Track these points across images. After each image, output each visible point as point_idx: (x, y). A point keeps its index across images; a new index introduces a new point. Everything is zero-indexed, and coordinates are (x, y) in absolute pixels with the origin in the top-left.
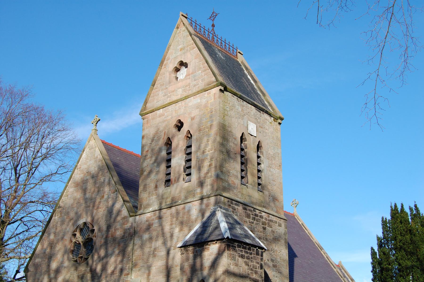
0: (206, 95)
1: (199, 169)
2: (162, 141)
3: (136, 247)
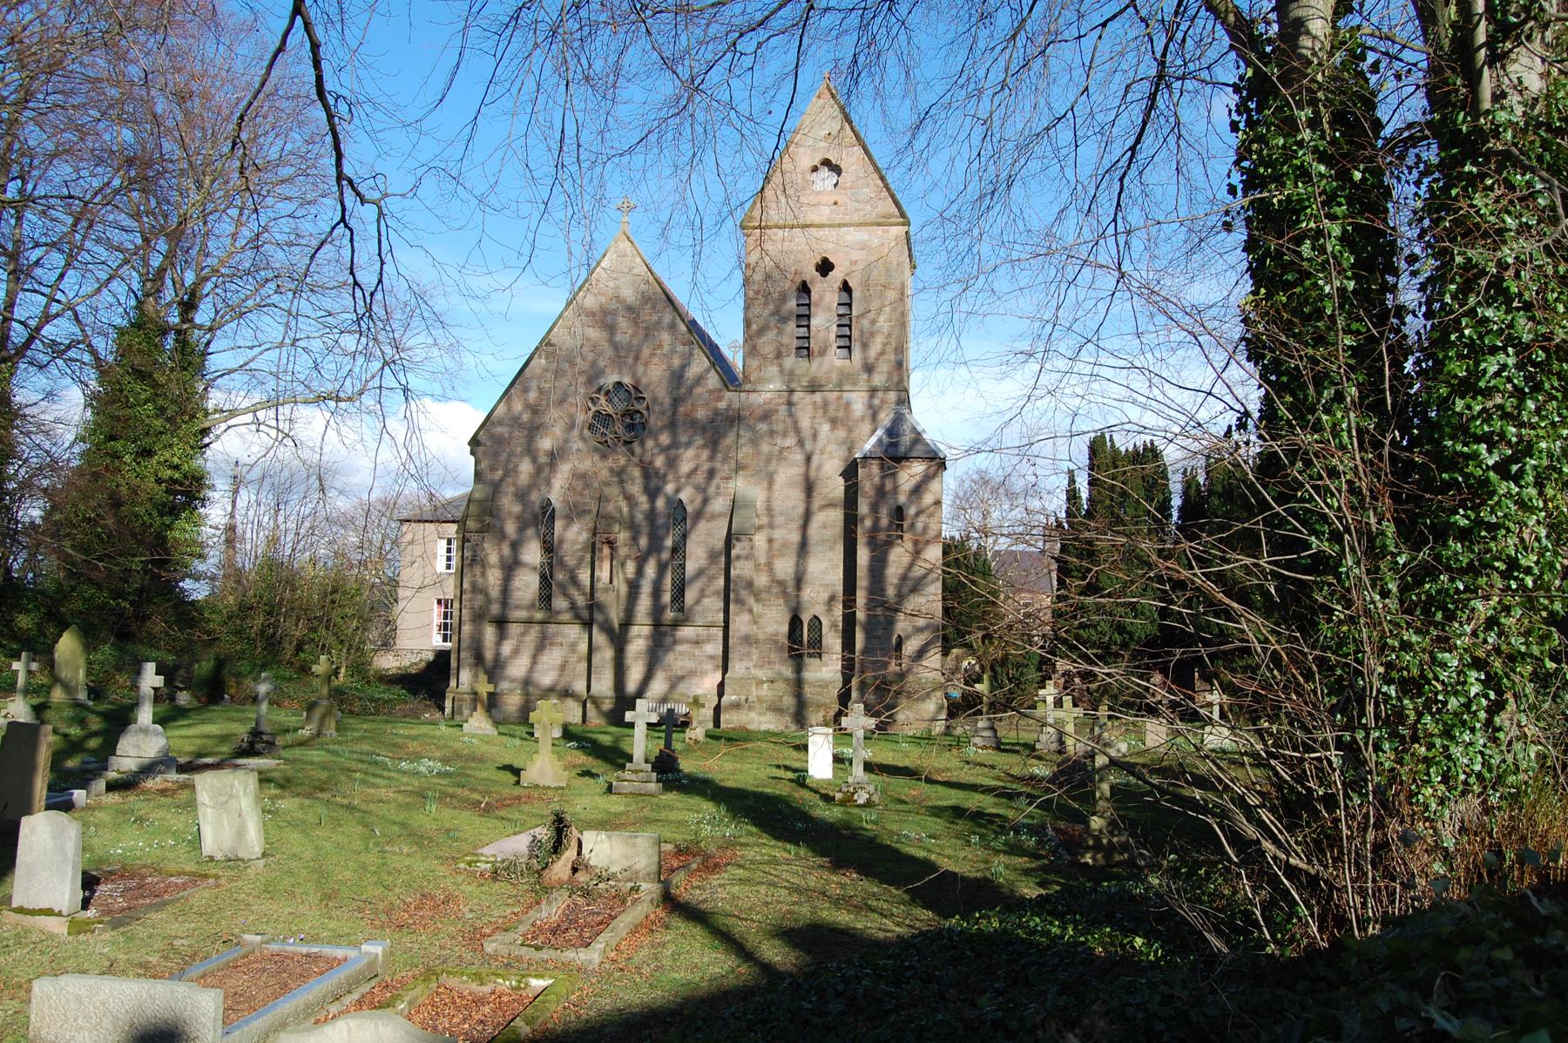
1: (865, 346)
3: (741, 441)
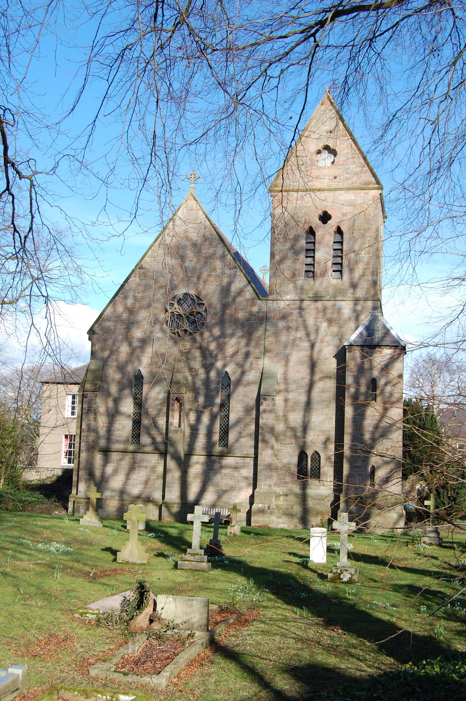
0: (362, 194)
1: (351, 270)
2: (301, 230)
3: (268, 333)
